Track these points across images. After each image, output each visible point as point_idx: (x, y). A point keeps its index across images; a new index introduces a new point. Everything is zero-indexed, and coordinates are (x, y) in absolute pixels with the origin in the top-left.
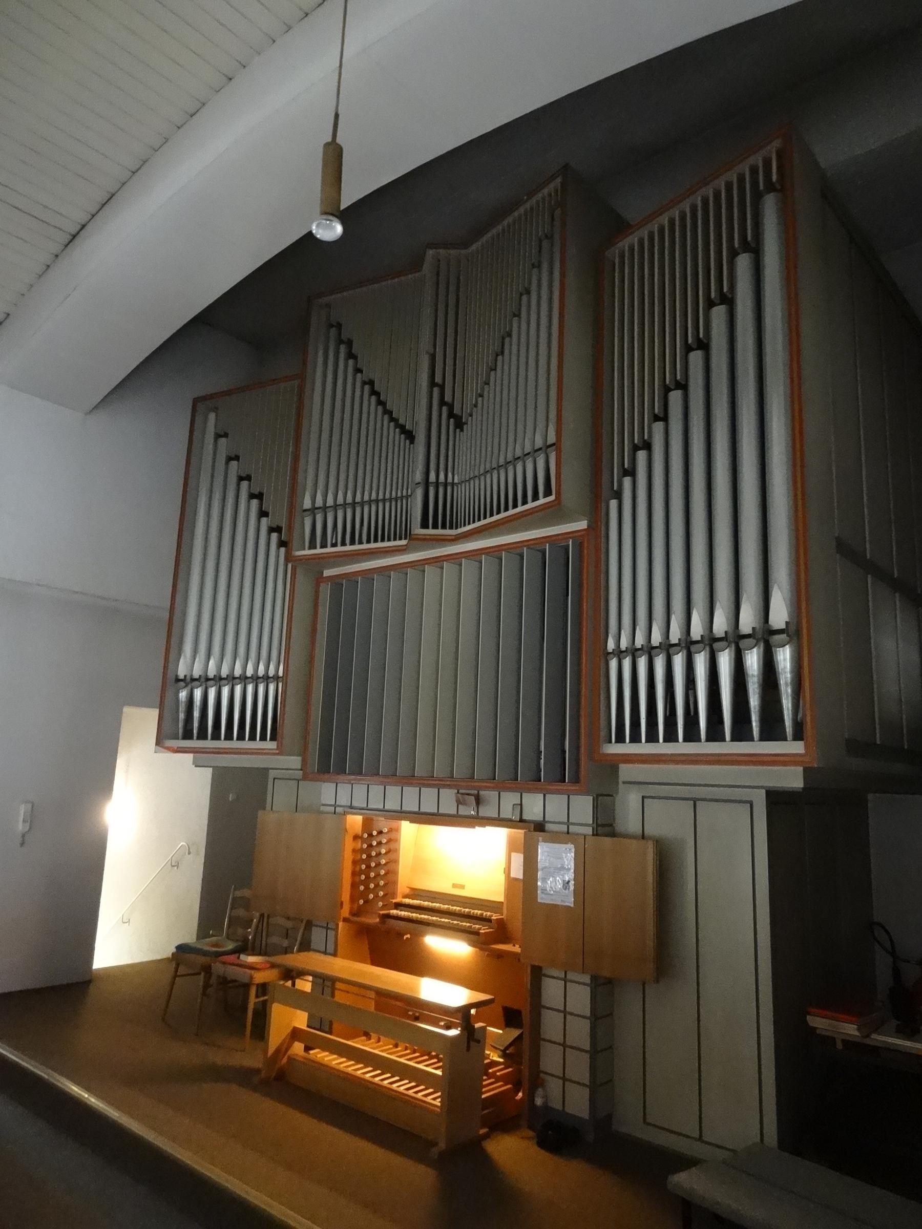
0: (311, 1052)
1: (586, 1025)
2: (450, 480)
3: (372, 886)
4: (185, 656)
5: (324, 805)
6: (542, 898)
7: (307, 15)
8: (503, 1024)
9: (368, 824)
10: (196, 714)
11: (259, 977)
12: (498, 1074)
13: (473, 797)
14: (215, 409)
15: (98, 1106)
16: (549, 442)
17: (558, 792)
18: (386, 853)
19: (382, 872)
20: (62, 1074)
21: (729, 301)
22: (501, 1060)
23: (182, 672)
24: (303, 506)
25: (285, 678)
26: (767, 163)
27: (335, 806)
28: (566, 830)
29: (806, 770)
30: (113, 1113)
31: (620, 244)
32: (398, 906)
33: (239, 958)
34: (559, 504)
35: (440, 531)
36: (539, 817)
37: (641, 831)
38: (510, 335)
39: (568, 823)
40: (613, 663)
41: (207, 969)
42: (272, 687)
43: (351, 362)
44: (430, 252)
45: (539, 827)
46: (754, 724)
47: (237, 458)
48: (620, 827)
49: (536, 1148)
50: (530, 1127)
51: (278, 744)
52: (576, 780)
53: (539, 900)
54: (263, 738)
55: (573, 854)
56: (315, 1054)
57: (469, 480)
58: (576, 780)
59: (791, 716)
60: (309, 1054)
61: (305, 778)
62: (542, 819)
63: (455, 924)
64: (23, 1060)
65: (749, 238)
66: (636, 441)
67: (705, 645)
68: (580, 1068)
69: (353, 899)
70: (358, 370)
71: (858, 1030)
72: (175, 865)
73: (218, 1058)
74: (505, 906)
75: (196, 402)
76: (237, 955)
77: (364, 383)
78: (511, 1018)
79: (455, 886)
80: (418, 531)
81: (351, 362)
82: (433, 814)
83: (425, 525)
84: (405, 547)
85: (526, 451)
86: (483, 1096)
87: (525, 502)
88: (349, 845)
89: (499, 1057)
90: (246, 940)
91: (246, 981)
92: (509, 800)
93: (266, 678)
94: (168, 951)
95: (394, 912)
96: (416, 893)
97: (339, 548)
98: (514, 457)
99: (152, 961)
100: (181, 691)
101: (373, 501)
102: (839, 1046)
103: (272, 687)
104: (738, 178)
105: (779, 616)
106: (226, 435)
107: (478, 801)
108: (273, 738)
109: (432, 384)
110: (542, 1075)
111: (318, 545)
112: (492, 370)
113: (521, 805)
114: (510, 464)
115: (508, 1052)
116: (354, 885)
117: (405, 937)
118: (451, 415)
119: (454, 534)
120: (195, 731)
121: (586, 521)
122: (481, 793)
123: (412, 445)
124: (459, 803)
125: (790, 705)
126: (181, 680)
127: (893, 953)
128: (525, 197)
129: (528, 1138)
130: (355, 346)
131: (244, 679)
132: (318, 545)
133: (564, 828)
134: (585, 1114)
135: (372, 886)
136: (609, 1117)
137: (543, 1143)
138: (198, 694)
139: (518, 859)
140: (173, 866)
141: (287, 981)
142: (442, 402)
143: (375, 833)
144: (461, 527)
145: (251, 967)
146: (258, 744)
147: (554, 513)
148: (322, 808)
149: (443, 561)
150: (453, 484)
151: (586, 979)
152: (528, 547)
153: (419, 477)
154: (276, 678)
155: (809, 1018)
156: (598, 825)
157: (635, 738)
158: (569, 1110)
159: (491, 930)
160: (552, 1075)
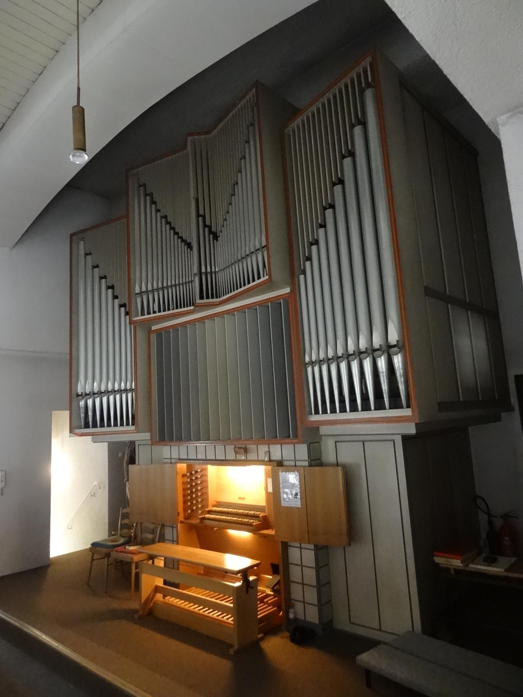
0: (167, 598)
1: (313, 572)
2: (213, 270)
3: (194, 502)
4: (81, 382)
5: (165, 459)
6: (283, 504)
7: (93, 10)
8: (272, 574)
9: (190, 468)
10: (90, 414)
11: (136, 558)
12: (269, 602)
13: (243, 450)
14: (83, 239)
15: (46, 640)
16: (263, 245)
17: (289, 443)
18: (201, 483)
19: (199, 494)
20: (29, 623)
21: (352, 154)
22: (272, 593)
23: (80, 391)
24: (135, 292)
25: (136, 390)
26: (365, 71)
27: (171, 459)
28: (294, 464)
29: (416, 424)
30: (54, 644)
31: (293, 124)
32: (209, 512)
33: (125, 548)
34: (271, 280)
35: (211, 300)
36: (279, 458)
37: (336, 462)
38: (237, 184)
39: (295, 460)
40: (309, 369)
41: (108, 555)
42: (130, 395)
43: (153, 206)
44: (190, 139)
45: (280, 464)
46: (385, 400)
47: (97, 266)
48: (324, 459)
49: (290, 643)
50: (288, 631)
51: (136, 427)
52: (296, 436)
53: (282, 505)
54: (128, 424)
55: (298, 477)
56: (168, 599)
57: (223, 270)
58: (296, 436)
59: (404, 394)
60: (165, 599)
61: (152, 444)
62: (281, 459)
63: (240, 521)
64: (8, 617)
65: (360, 117)
66: (334, 180)
67: (356, 356)
68: (312, 596)
69: (185, 510)
70: (158, 211)
71: (462, 562)
72: (93, 495)
73: (115, 605)
74: (266, 508)
75: (72, 236)
76: (123, 547)
77: (162, 217)
78: (275, 570)
79: (240, 498)
80: (198, 301)
81: (153, 206)
82: (223, 460)
83: (201, 298)
84: (193, 311)
85: (257, 248)
86: (259, 617)
87: (254, 280)
88: (180, 481)
89: (271, 591)
90: (130, 537)
91: (130, 561)
92: (263, 449)
93: (126, 390)
94: (89, 546)
95: (207, 516)
96: (219, 504)
97: (158, 314)
98: (245, 254)
99: (85, 549)
100: (80, 401)
101: (173, 285)
102: (452, 572)
103: (130, 395)
104: (351, 81)
105: (394, 337)
106: (90, 254)
107: (246, 451)
108: (133, 424)
109: (198, 215)
110: (292, 601)
111: (146, 313)
112: (232, 195)
113: (269, 452)
114: (248, 256)
115: (275, 588)
116: (185, 502)
117: (215, 529)
118: (210, 232)
119: (218, 301)
120: (91, 423)
121: (289, 288)
122: (247, 446)
123: (191, 252)
124: (236, 452)
125: (403, 388)
126: (80, 395)
127: (488, 513)
128: (238, 102)
129: (286, 637)
130: (154, 195)
131: (114, 392)
132: (146, 313)
133: (293, 463)
134: (316, 621)
135: (194, 502)
136: (331, 622)
137: (294, 640)
138: (90, 402)
139: (270, 480)
140: (92, 496)
141: (149, 561)
142: (205, 226)
143: (193, 472)
144: (222, 297)
145: (132, 553)
146: (125, 428)
147: (270, 285)
148: (164, 460)
149: (215, 317)
150: (215, 272)
151: (312, 547)
152: (259, 305)
153: (195, 270)
154: (131, 390)
155: (435, 558)
156: (311, 460)
157: (325, 411)
158: (308, 619)
159: (260, 522)
160: (482, 510)
